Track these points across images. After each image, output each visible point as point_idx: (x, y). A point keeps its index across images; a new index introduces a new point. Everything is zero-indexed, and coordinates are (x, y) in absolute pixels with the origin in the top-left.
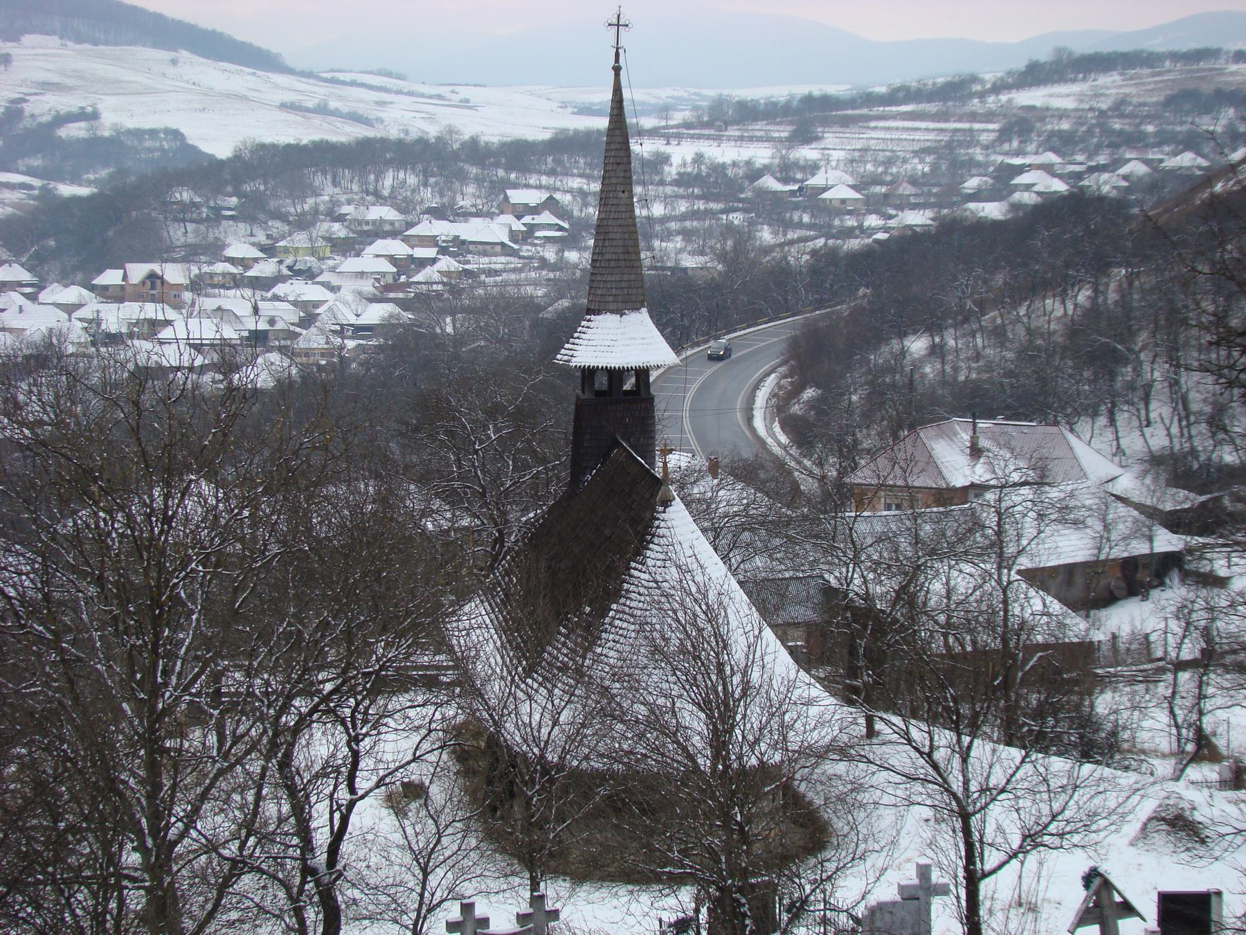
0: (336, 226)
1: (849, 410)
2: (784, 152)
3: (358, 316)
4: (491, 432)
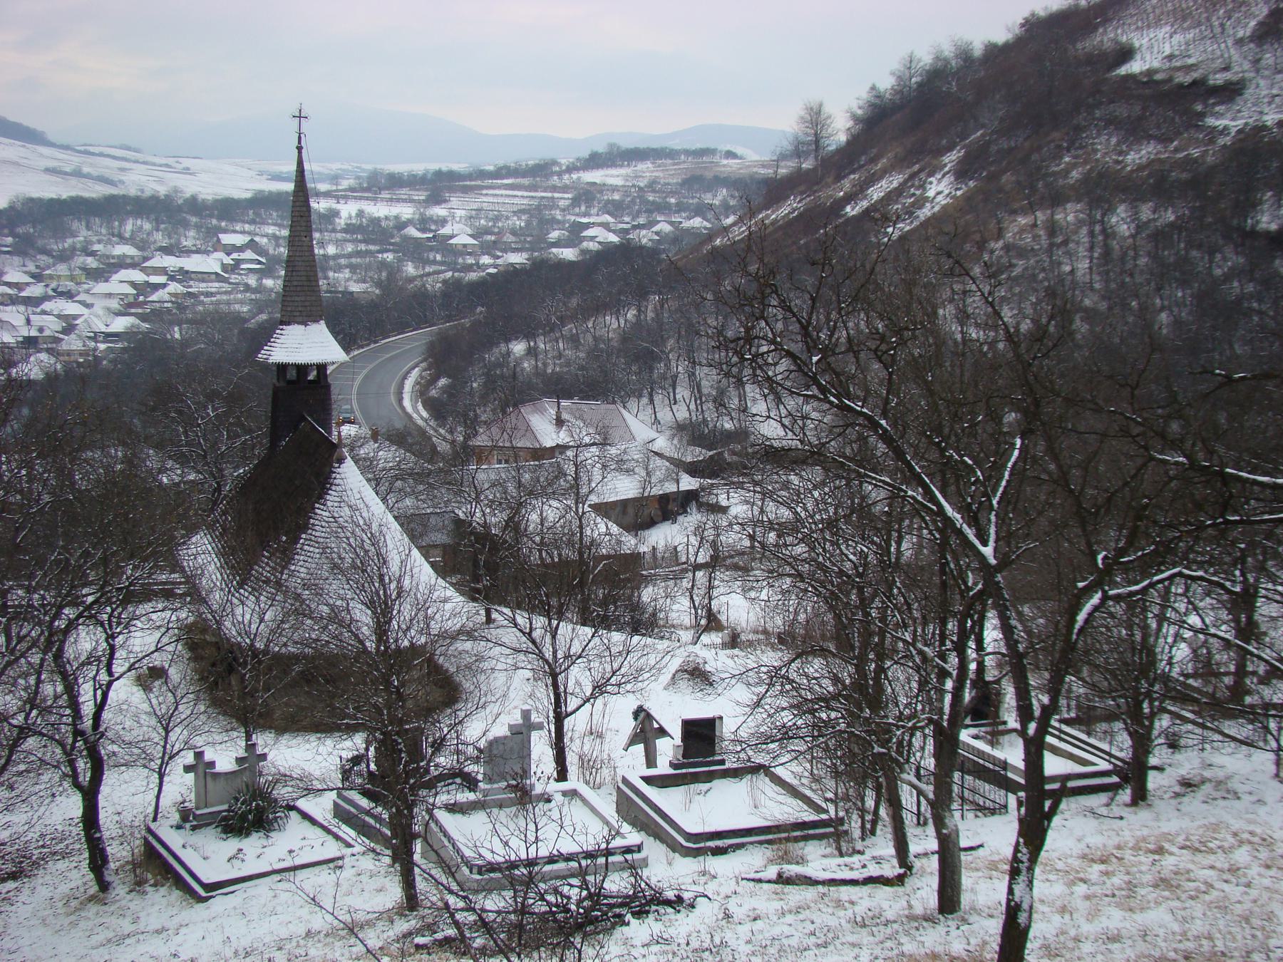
0: (90, 260)
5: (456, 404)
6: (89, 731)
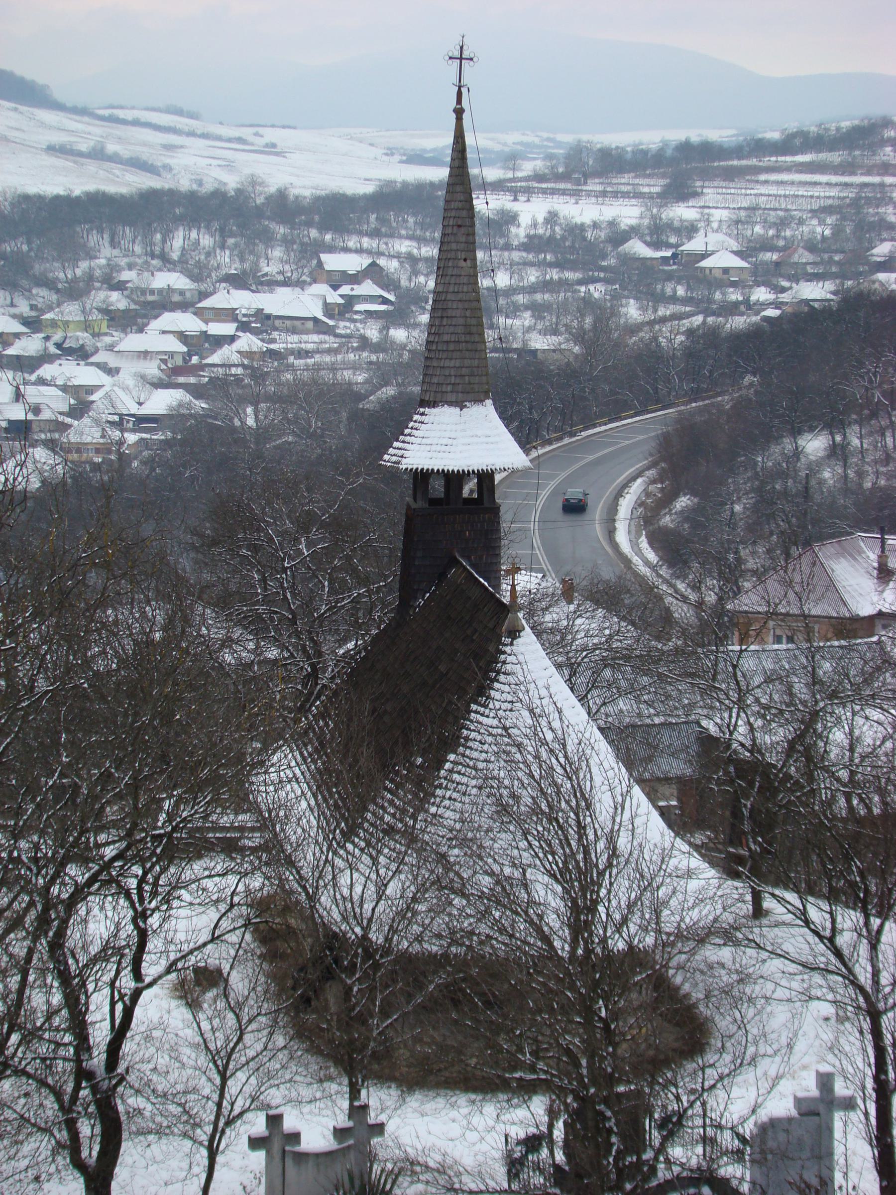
0: (115, 296)
5: (706, 539)
6: (101, 1071)
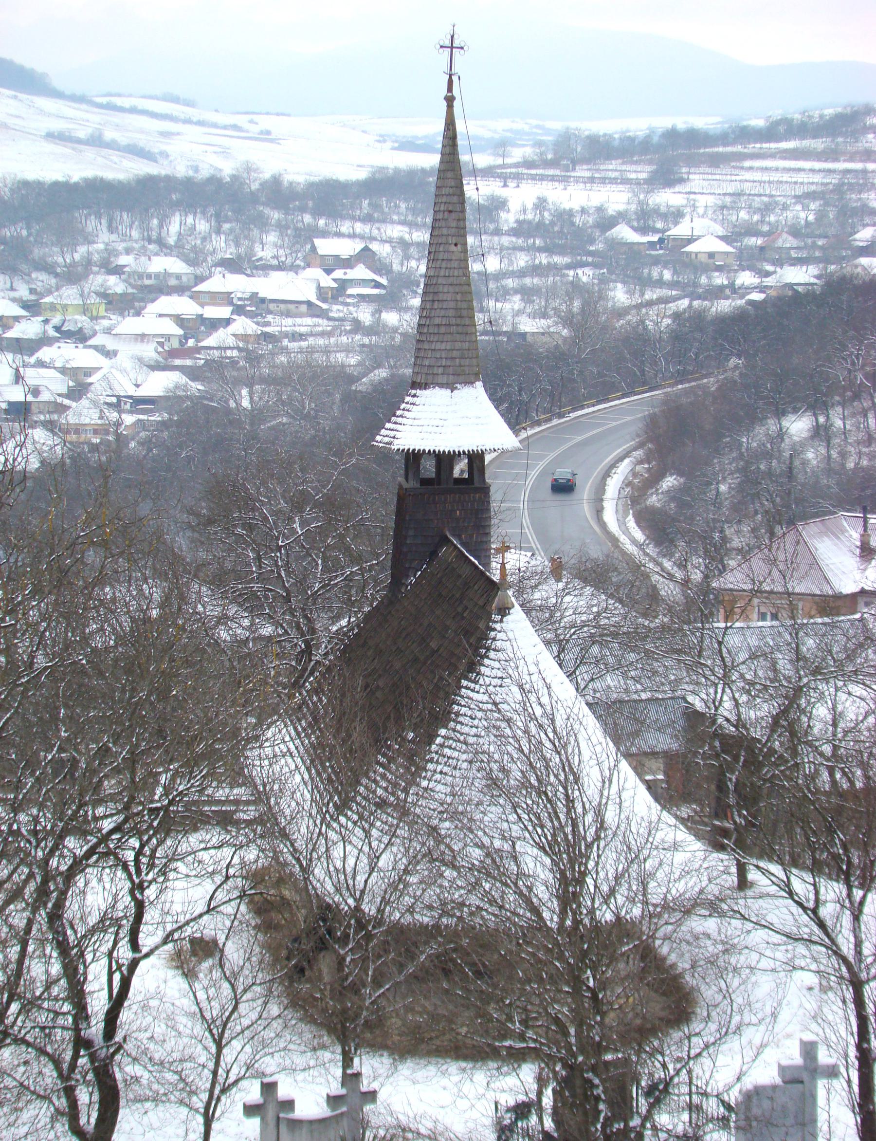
0: (112, 280)
1: (717, 502)
2: (642, 197)
3: (137, 386)
4: (297, 526)
5: (692, 518)
